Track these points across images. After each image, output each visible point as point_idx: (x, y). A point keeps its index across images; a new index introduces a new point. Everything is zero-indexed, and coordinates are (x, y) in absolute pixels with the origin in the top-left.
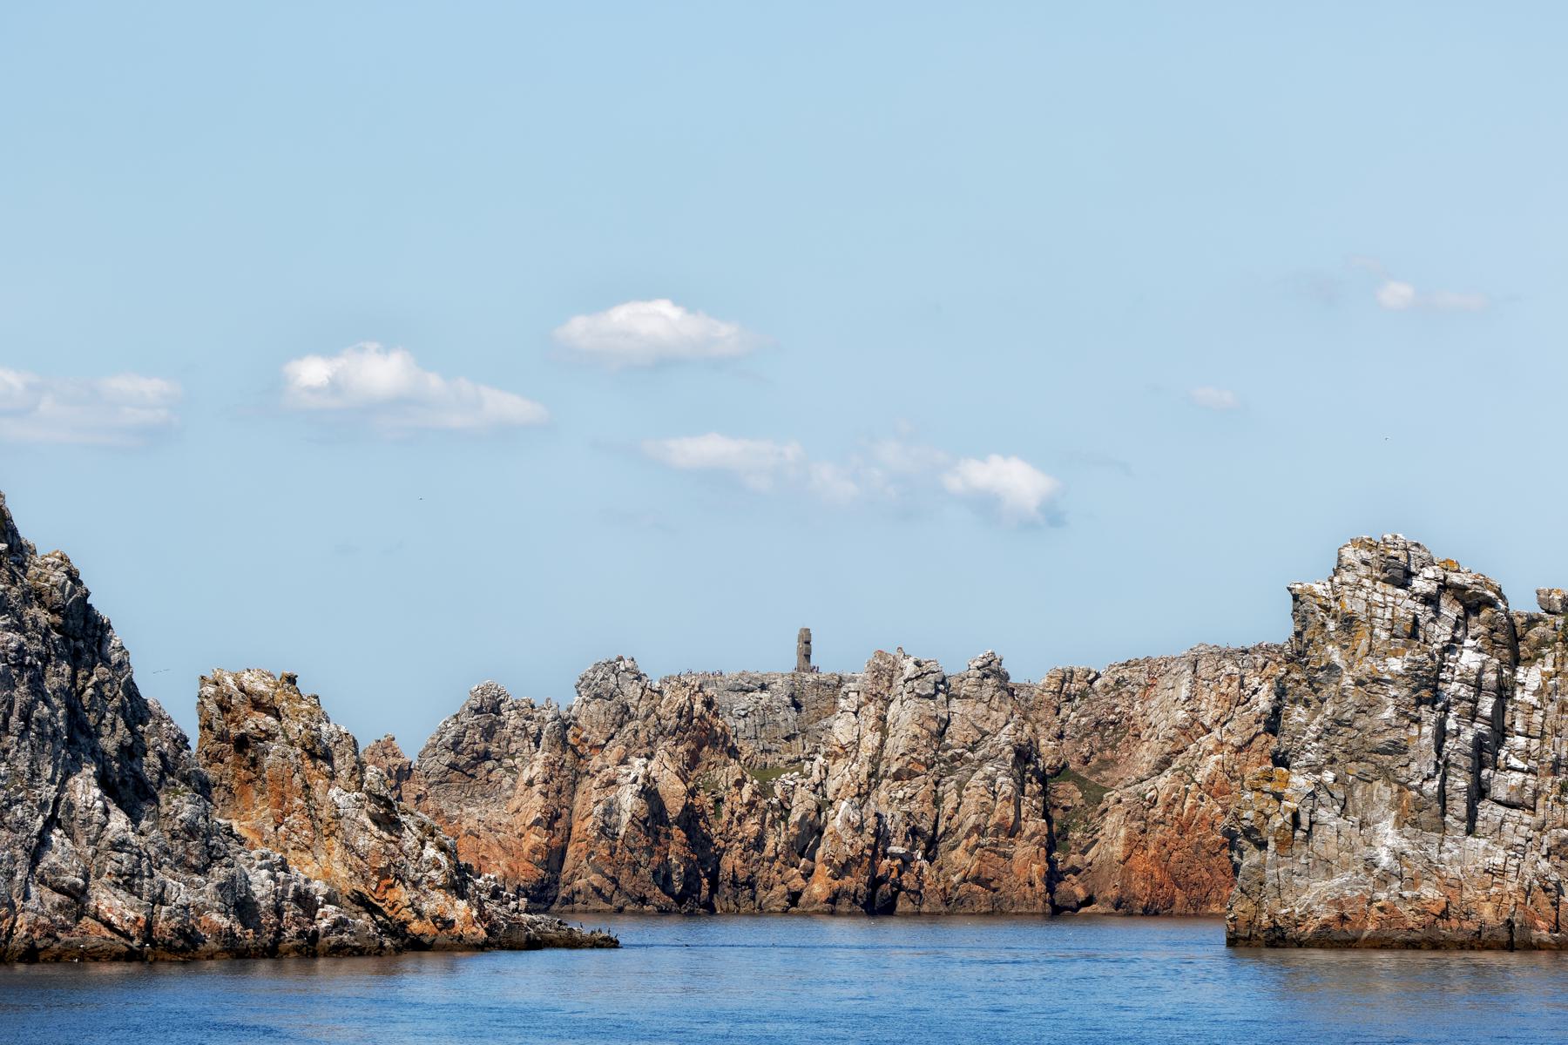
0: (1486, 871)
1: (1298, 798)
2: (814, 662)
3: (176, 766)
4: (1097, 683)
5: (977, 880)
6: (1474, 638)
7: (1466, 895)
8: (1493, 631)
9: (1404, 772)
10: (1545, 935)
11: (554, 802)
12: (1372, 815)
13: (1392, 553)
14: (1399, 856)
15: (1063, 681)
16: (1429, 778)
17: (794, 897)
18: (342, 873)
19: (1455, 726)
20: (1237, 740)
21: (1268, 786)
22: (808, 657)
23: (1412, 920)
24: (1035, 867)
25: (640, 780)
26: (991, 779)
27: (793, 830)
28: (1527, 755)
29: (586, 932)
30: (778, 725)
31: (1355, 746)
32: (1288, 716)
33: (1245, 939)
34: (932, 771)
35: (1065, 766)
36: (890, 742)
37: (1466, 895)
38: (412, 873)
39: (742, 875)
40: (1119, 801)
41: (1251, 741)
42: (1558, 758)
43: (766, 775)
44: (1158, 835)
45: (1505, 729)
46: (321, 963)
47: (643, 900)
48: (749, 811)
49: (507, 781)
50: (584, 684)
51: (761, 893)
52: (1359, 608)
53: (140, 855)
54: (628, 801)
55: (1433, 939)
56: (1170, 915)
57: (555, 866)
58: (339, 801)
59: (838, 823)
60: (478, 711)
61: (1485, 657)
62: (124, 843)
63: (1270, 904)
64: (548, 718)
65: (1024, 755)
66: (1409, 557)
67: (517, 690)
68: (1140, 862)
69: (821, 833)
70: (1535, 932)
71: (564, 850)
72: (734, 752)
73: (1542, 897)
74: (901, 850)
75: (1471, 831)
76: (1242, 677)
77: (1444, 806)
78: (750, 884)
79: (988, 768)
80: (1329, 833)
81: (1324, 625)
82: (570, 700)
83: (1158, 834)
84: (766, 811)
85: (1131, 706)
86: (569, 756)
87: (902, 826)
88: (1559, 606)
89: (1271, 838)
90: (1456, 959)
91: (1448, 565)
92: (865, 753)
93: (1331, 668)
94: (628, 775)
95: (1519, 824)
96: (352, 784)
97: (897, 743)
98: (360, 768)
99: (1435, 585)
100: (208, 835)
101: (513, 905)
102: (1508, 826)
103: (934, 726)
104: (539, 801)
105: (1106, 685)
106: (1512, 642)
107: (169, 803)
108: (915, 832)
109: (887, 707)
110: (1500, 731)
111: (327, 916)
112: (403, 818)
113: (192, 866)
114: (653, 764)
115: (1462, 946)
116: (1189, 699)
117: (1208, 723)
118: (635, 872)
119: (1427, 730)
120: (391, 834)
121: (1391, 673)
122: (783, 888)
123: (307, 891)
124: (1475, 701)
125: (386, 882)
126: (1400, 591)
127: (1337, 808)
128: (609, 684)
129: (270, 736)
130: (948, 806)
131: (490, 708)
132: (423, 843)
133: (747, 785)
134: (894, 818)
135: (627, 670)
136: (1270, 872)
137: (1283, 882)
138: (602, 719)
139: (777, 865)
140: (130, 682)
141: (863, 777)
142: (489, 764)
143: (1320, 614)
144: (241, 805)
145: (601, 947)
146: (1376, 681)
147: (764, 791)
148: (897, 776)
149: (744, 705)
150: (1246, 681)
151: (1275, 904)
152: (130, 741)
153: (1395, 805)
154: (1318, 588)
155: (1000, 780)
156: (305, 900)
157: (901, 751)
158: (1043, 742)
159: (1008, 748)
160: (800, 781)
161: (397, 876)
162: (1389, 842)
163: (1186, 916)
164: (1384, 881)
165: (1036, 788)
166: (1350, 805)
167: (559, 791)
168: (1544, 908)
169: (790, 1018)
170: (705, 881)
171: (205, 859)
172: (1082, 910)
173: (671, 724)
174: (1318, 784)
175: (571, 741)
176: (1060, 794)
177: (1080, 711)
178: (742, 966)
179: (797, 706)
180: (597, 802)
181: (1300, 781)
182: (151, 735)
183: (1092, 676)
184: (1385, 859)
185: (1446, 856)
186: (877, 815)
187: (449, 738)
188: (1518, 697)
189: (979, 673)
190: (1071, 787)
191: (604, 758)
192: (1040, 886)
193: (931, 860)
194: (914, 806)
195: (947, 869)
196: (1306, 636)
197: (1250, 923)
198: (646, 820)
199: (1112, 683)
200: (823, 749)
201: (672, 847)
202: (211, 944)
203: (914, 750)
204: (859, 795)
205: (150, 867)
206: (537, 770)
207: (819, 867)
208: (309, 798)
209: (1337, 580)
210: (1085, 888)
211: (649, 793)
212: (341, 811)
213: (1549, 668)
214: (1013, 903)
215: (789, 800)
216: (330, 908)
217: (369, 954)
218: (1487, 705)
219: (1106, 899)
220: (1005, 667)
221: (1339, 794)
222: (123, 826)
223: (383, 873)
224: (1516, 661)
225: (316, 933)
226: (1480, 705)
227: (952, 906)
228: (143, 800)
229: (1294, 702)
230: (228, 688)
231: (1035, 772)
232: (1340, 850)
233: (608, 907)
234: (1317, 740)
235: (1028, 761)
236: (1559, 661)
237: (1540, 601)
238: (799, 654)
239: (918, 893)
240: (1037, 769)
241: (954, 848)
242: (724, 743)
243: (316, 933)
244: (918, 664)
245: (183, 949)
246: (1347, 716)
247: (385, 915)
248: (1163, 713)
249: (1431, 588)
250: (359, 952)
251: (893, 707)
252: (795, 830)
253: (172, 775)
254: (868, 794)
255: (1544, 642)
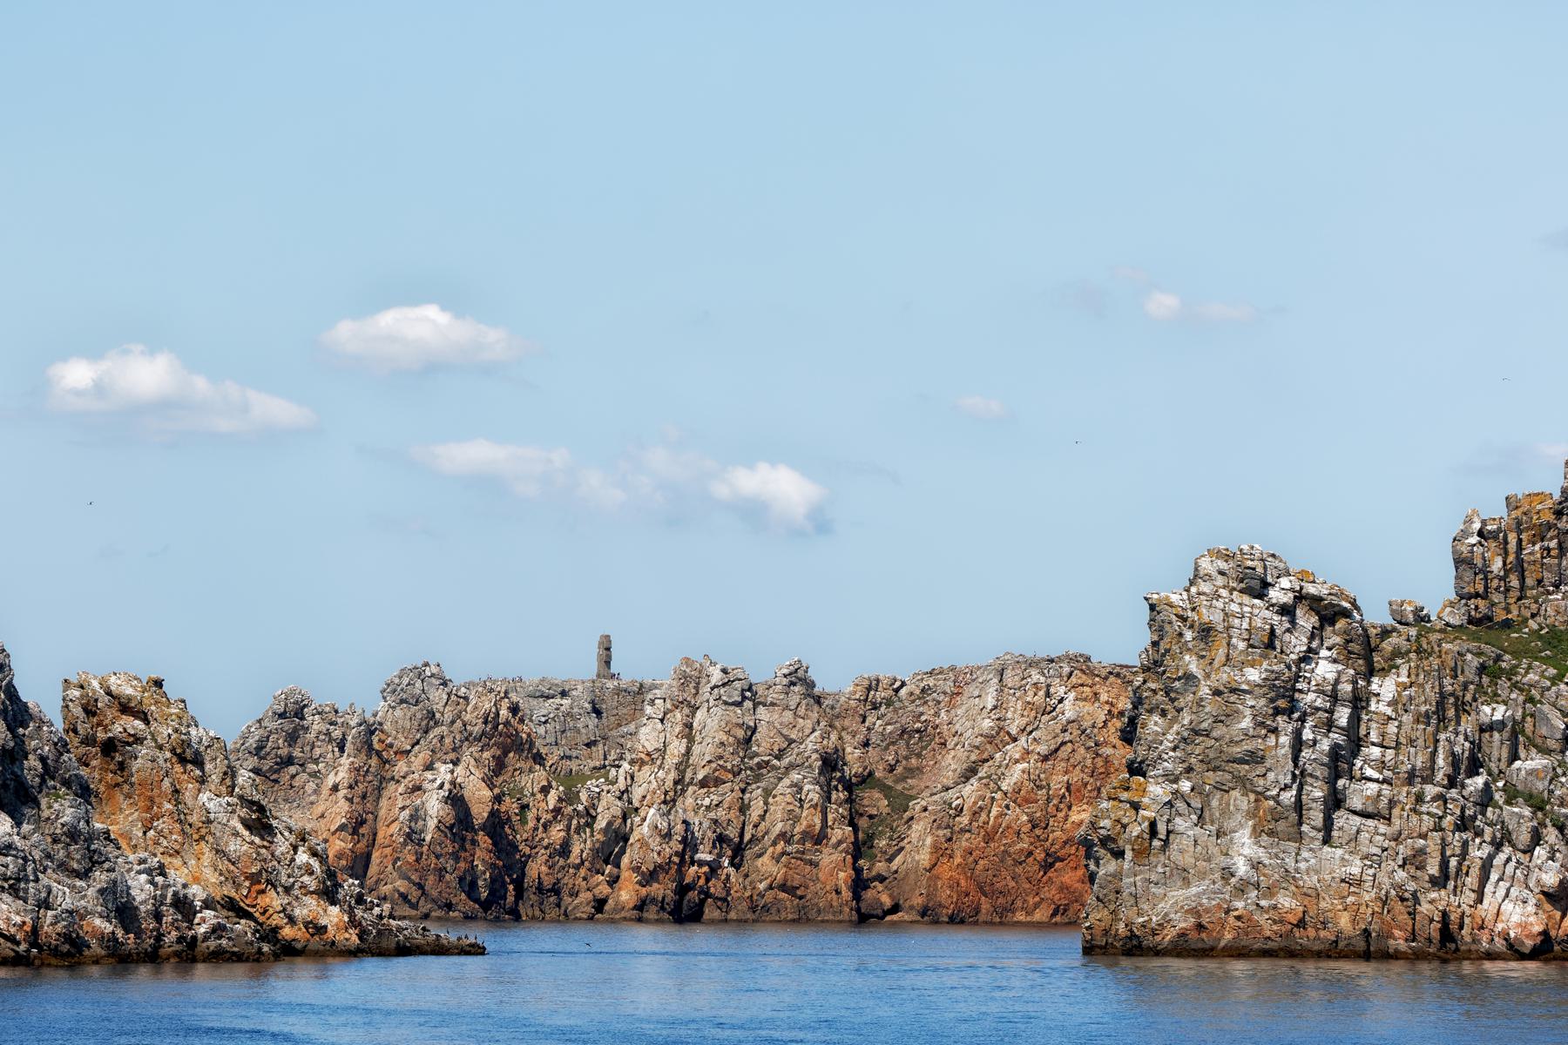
0: (1343, 881)
1: (1156, 807)
2: (614, 670)
3: (57, 769)
4: (903, 692)
5: (783, 887)
6: (1329, 649)
7: (1323, 905)
8: (1348, 642)
9: (1261, 782)
10: (1401, 945)
11: (360, 808)
12: (1229, 824)
13: (1249, 563)
14: (1256, 865)
15: (869, 689)
16: (1286, 787)
17: (600, 904)
18: (213, 878)
19: (1311, 736)
20: (1043, 749)
21: (1125, 796)
22: (608, 663)
23: (1268, 929)
24: (842, 875)
25: (447, 786)
26: (798, 787)
27: (598, 836)
28: (1381, 765)
29: (453, 938)
30: (578, 731)
31: (1212, 755)
32: (1144, 726)
33: (1101, 947)
34: (738, 779)
35: (871, 774)
36: (696, 749)
37: (1323, 905)
38: (284, 879)
39: (548, 882)
40: (925, 809)
41: (1057, 750)
42: (1414, 769)
43: (571, 781)
44: (964, 844)
45: (1360, 739)
46: (201, 968)
47: (449, 906)
48: (555, 818)
49: (311, 786)
50: (390, 689)
51: (567, 899)
52: (1216, 618)
53: (25, 859)
54: (434, 806)
55: (1293, 947)
56: (976, 923)
57: (360, 872)
58: (211, 806)
59: (645, 829)
60: (282, 716)
61: (1340, 667)
62: (10, 846)
63: (1127, 913)
64: (353, 723)
65: (831, 763)
66: (1265, 568)
67: (320, 697)
68: (945, 870)
69: (626, 839)
70: (1392, 942)
71: (368, 856)
72: (539, 759)
73: (1399, 907)
74: (709, 858)
75: (1327, 841)
76: (1049, 686)
77: (1301, 816)
78: (556, 890)
79: (795, 776)
80: (1186, 842)
81: (1181, 635)
82: (374, 705)
83: (964, 842)
84: (571, 818)
85: (937, 714)
86: (374, 761)
87: (709, 833)
88: (1411, 618)
89: (1128, 848)
90: (1309, 968)
91: (1304, 576)
92: (672, 760)
93: (1189, 678)
94: (434, 781)
95: (1374, 835)
96: (223, 789)
97: (704, 751)
98: (230, 773)
99: (1291, 595)
100: (90, 839)
101: (377, 910)
102: (1364, 836)
103: (740, 733)
104: (344, 806)
105: (912, 694)
106: (1366, 653)
107: (50, 807)
108: (721, 839)
109: (694, 714)
110: (1356, 742)
111: (206, 920)
112: (274, 823)
113: (74, 871)
114: (459, 770)
115: (1319, 955)
116: (995, 707)
117: (1014, 732)
118: (441, 878)
119: (1284, 740)
120: (263, 839)
121: (1248, 683)
122: (589, 895)
123: (185, 896)
124: (1331, 712)
125: (257, 887)
126: (1257, 601)
127: (1194, 817)
128: (414, 690)
129: (138, 740)
130: (755, 813)
131: (294, 712)
132: (295, 848)
133: (553, 792)
134: (701, 826)
135: (433, 675)
136: (1127, 880)
137: (1140, 891)
138: (408, 724)
139: (583, 872)
140: (10, 685)
141: (669, 784)
142: (292, 769)
143: (1177, 624)
144: (107, 810)
145: (468, 953)
146: (1233, 691)
147: (570, 797)
148: (703, 784)
149: (544, 712)
150: (1052, 690)
151: (1132, 913)
152: (12, 744)
153: (1252, 814)
154: (1174, 598)
155: (806, 788)
156: (183, 906)
157: (707, 758)
158: (849, 750)
159: (815, 756)
160: (605, 788)
161: (268, 882)
162: (1246, 851)
163: (991, 923)
164: (1241, 890)
165: (842, 795)
166: (1207, 814)
167: (364, 797)
168: (1400, 918)
169: (733, 1027)
170: (511, 887)
171: (86, 864)
172: (888, 918)
173: (477, 730)
174: (1176, 793)
175: (376, 746)
176: (865, 802)
177: (886, 719)
178: (543, 972)
179: (598, 712)
180: (403, 808)
181: (1157, 791)
182: (32, 738)
183: (898, 684)
184: (1242, 869)
185: (1302, 865)
186: (684, 822)
187: (252, 742)
188: (1373, 707)
189: (785, 681)
190: (877, 795)
191: (409, 763)
192: (847, 894)
193: (737, 867)
194: (721, 814)
195: (753, 876)
196: (1163, 646)
197: (1106, 932)
198: (452, 826)
199: (918, 692)
200: (628, 756)
201: (478, 853)
202: (96, 948)
203: (721, 757)
204: (665, 802)
205: (35, 871)
206: (342, 775)
207: (625, 874)
208: (178, 803)
209: (1193, 590)
210: (890, 896)
211: (455, 799)
212: (212, 816)
213: (1404, 679)
214: (819, 911)
215: (594, 807)
216: (208, 913)
217: (247, 960)
218: (1343, 716)
219: (912, 908)
220: (812, 675)
221: (1196, 803)
222: (9, 829)
223: (254, 879)
224: (1370, 672)
225: (194, 938)
226: (1336, 715)
227: (759, 913)
228: (24, 804)
229: (1150, 711)
230: (94, 691)
231: (841, 780)
232: (1197, 859)
233: (414, 912)
234: (1174, 749)
235: (834, 769)
236: (1413, 671)
237: (1393, 612)
238: (599, 661)
239: (725, 900)
240: (843, 776)
241: (760, 855)
242: (530, 749)
243: (194, 938)
244: (724, 671)
245: (69, 954)
246: (1205, 725)
247: (255, 920)
248: (969, 721)
249: (1287, 598)
250: (238, 958)
251: (699, 714)
252: (600, 837)
253: (53, 778)
254: (674, 801)
255: (1397, 653)
